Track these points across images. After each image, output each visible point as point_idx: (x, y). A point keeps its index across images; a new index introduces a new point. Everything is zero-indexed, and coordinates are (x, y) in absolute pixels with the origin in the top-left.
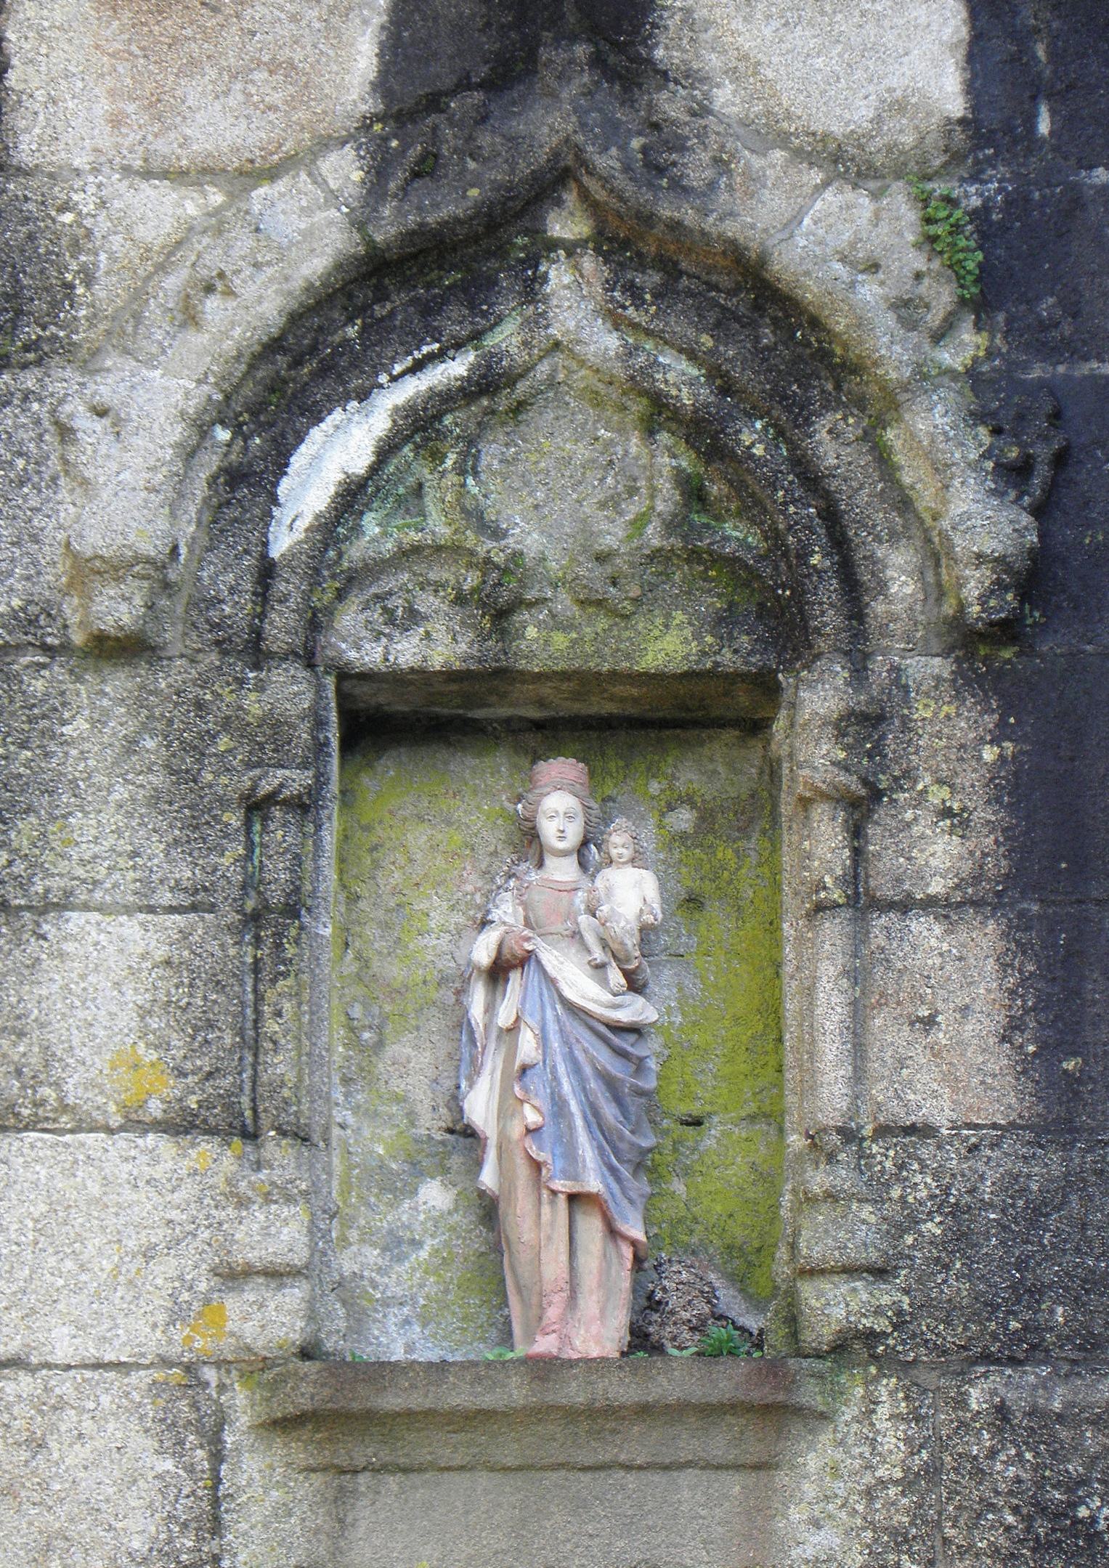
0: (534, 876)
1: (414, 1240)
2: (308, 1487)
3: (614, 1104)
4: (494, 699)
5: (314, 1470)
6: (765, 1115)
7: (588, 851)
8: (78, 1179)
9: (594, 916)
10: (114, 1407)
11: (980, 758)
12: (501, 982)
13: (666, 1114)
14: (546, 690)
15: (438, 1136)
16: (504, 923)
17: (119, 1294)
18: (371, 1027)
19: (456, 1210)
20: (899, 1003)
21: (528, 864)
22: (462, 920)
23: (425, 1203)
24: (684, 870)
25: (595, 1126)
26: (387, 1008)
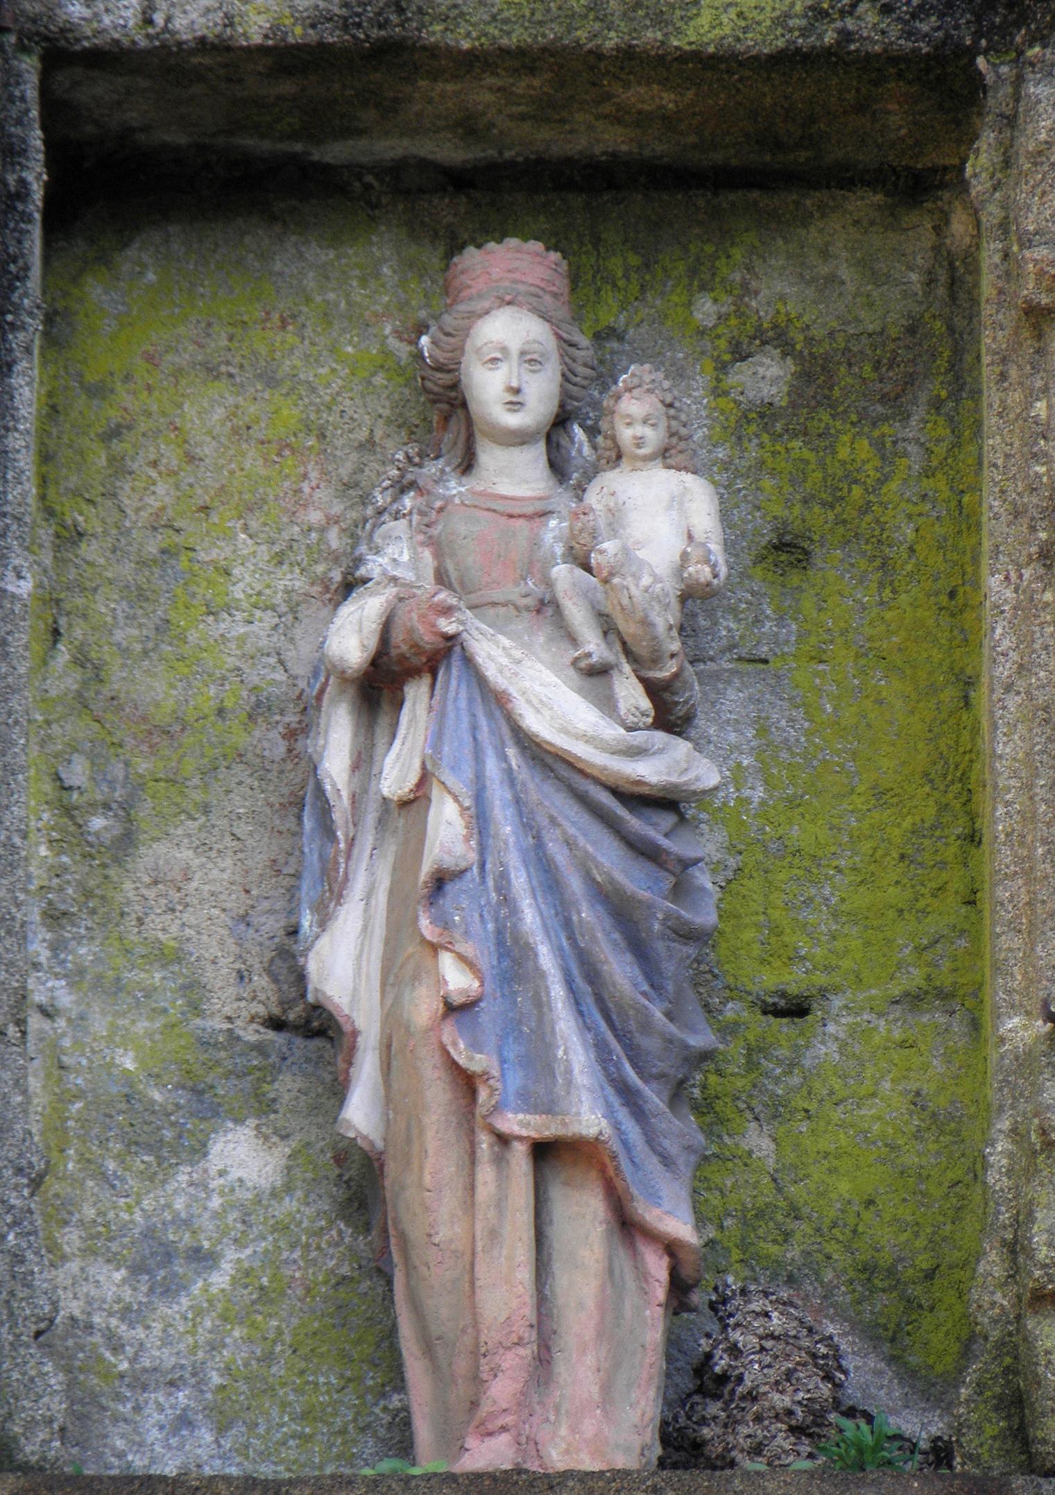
0: (455, 487)
1: (197, 1250)
3: (629, 957)
4: (369, 116)
6: (945, 995)
7: (570, 435)
9: (587, 568)
12: (385, 706)
13: (734, 992)
14: (482, 95)
15: (251, 1034)
16: (394, 579)
18: (107, 806)
19: (288, 1188)
21: (441, 463)
22: (300, 584)
23: (222, 1173)
24: (768, 483)
25: (590, 1001)
26: (143, 766)
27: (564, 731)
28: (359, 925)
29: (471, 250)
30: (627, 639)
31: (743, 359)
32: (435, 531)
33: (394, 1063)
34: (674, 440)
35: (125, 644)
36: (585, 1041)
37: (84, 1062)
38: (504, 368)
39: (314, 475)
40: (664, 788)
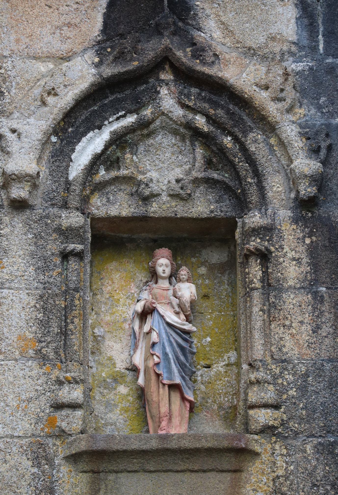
0: (154, 286)
2: (85, 478)
5: (85, 472)
7: (174, 276)
8: (6, 376)
10: (17, 451)
11: (304, 242)
17: (19, 414)
20: (279, 320)
23: (119, 392)
27: (173, 321)
38: (162, 267)
39: (133, 285)
40: (189, 330)
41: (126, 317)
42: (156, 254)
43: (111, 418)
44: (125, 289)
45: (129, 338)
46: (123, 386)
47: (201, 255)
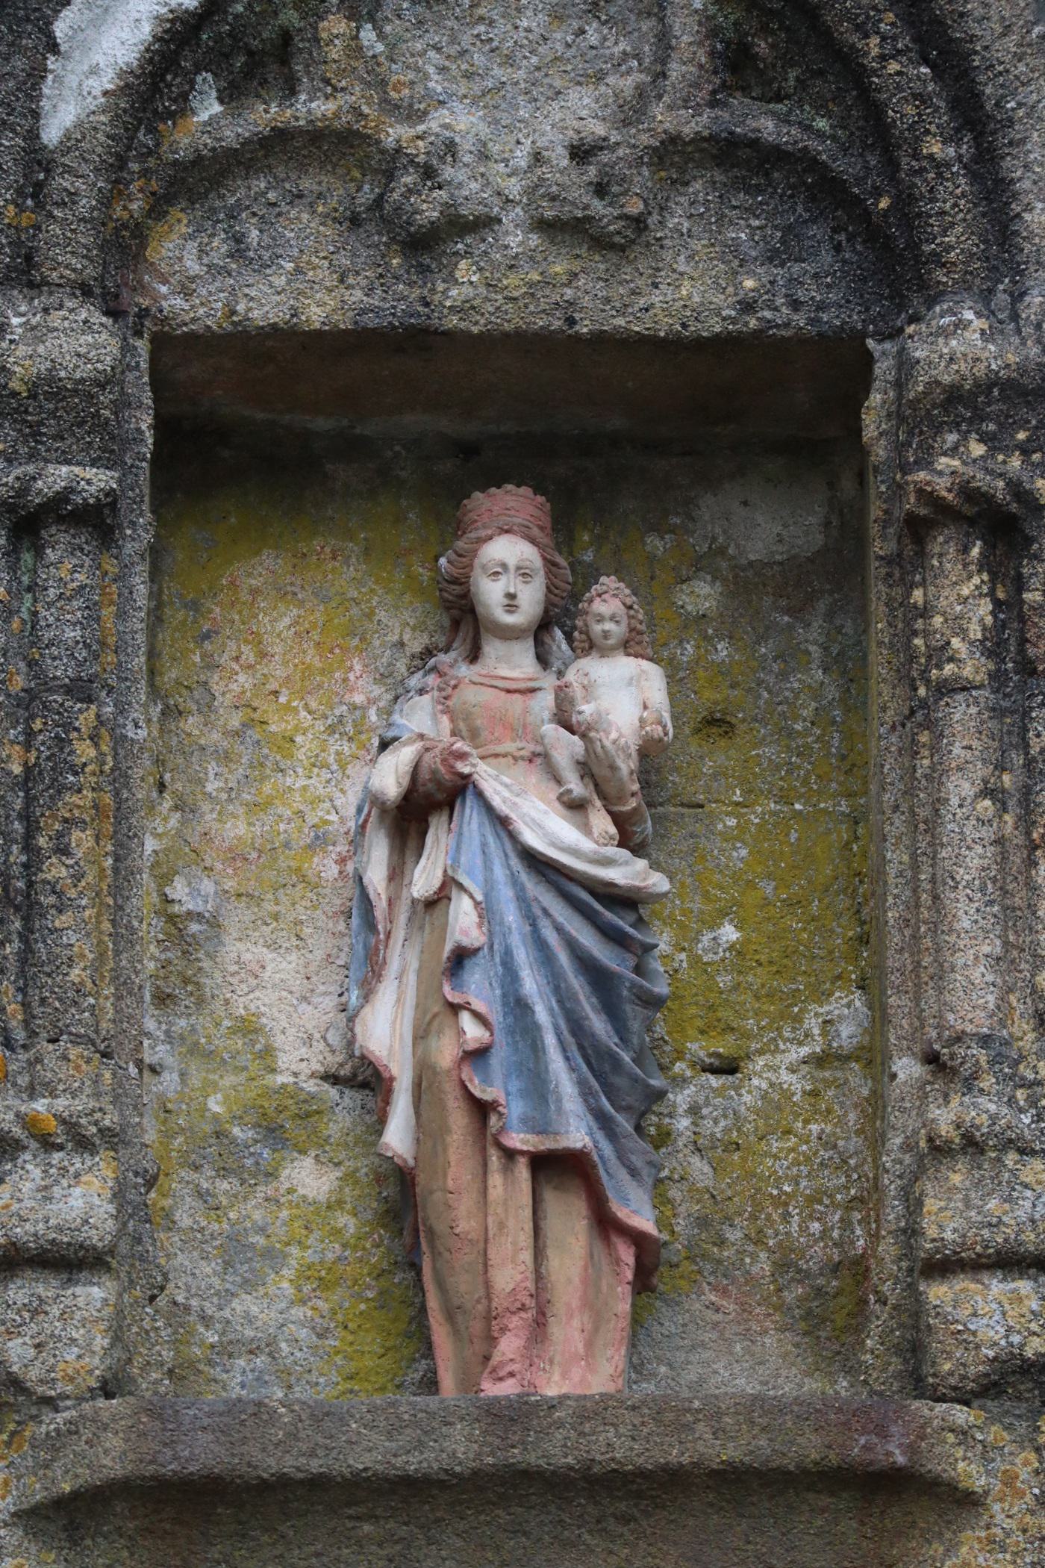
0: (464, 670)
3: (604, 1017)
7: (559, 626)
23: (291, 1191)
25: (574, 1048)
27: (553, 845)
28: (395, 997)
29: (477, 495)
30: (599, 781)
31: (683, 582)
32: (449, 703)
33: (424, 1097)
34: (634, 634)
35: (214, 794)
36: (571, 1079)
37: (184, 1107)
38: (503, 579)
39: (358, 667)
41: (326, 822)
42: (473, 516)
43: (249, 1319)
44: (320, 686)
45: (341, 926)
46: (308, 1162)
47: (693, 519)
